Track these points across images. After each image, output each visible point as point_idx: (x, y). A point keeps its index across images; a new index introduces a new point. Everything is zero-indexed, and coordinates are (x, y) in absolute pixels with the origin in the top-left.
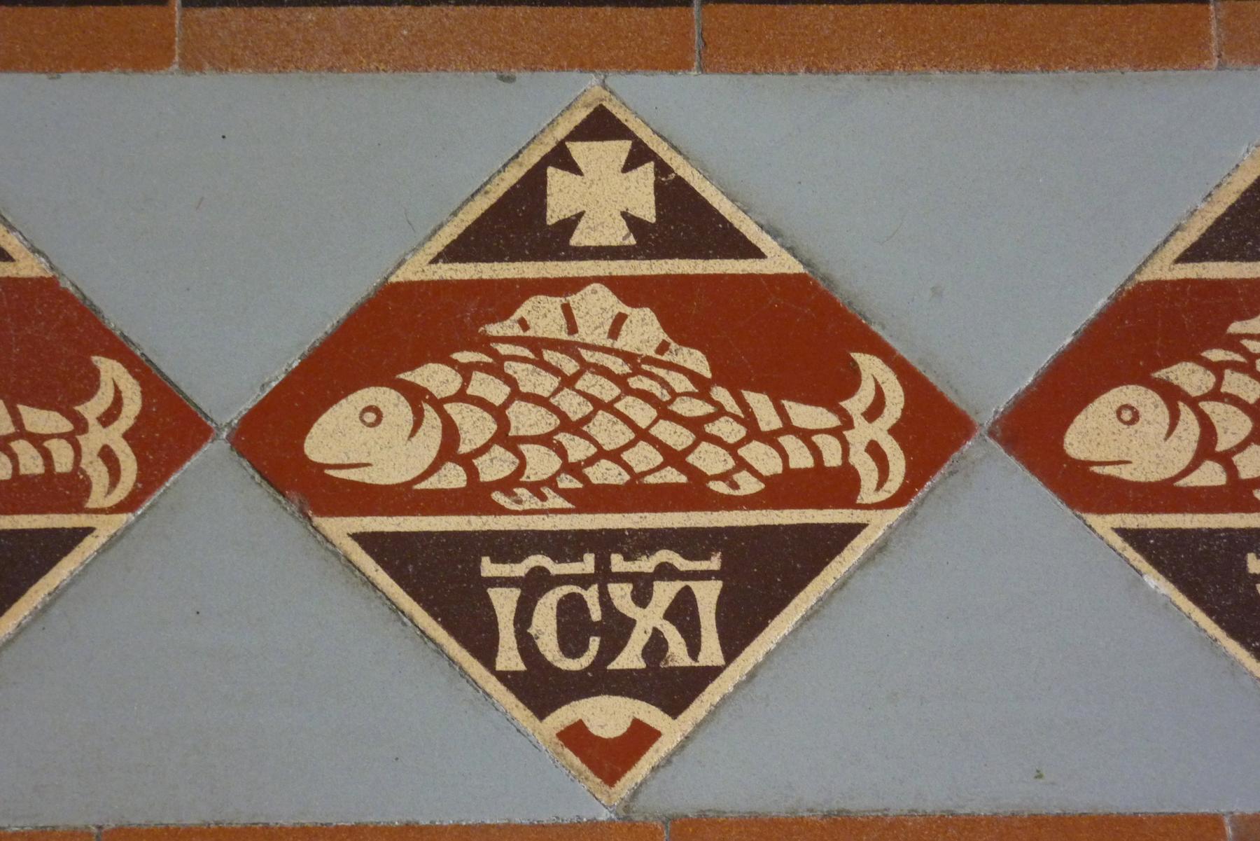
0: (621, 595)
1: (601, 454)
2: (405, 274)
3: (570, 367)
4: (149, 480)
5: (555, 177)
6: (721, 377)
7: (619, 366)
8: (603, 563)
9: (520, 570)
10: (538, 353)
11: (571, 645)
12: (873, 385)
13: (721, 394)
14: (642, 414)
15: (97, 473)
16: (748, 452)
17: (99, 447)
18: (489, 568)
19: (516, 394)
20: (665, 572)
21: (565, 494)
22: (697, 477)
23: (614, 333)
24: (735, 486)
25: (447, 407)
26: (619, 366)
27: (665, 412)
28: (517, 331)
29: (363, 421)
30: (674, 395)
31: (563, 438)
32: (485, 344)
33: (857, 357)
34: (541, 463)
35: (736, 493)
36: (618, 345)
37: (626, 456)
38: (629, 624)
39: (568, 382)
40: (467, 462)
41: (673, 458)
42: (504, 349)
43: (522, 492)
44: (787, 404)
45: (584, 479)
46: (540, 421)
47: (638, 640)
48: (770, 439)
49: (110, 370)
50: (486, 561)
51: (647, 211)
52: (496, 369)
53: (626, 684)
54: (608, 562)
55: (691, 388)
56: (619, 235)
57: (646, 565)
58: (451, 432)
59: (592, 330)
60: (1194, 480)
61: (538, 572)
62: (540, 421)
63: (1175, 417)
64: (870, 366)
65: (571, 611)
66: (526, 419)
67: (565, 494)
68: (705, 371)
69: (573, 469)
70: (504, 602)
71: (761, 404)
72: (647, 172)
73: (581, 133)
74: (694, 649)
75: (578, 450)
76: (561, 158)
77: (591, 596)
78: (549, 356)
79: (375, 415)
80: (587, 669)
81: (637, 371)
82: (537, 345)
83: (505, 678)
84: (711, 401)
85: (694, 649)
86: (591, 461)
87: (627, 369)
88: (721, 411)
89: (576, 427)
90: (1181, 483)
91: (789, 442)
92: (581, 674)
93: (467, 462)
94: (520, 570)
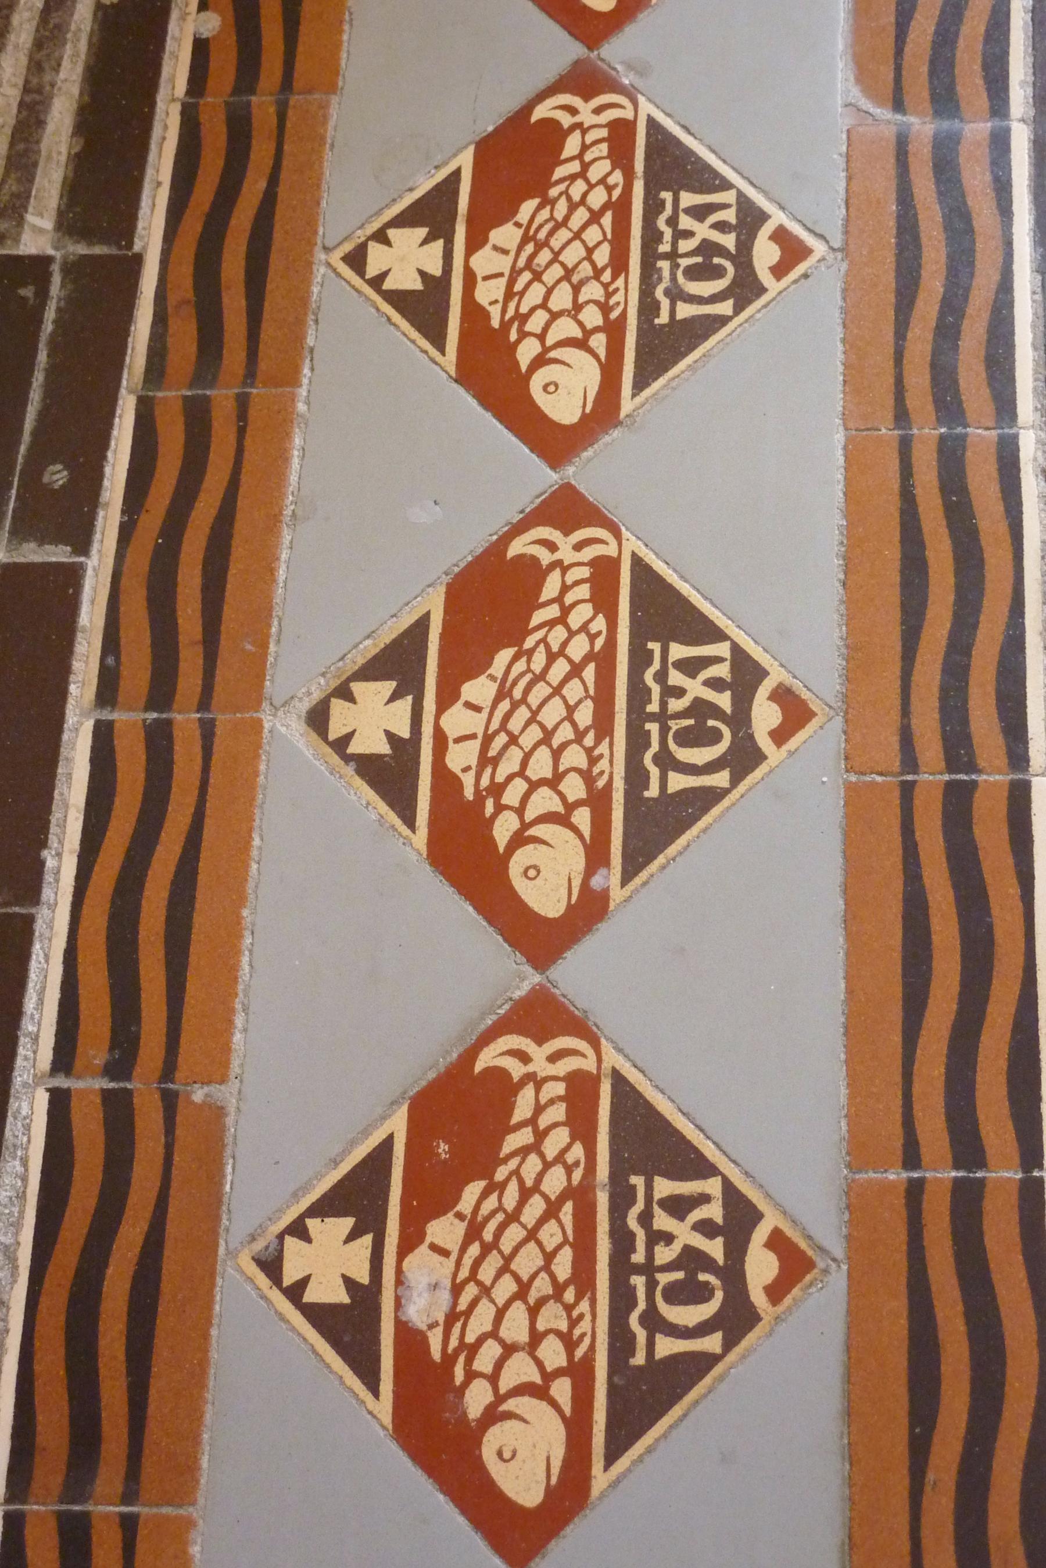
0: (664, 1255)
1: (570, 718)
2: (387, 1419)
3: (502, 739)
4: (615, 87)
5: (310, 1296)
6: (487, 1173)
7: (474, 1250)
8: (638, 1269)
9: (654, 772)
10: (516, 294)
11: (702, 1295)
12: (553, 111)
13: (501, 1173)
14: (514, 1234)
15: (564, 1067)
16: (550, 1153)
17: (573, 552)
18: (653, 791)
19: (494, 1334)
20: (645, 1218)
21: (614, 278)
22: (588, 658)
23: (445, 1253)
24: (577, 1164)
25: (502, 1391)
26: (474, 1250)
27: (542, 677)
28: (439, 1331)
29: (535, 878)
30: (500, 1208)
31: (533, 1297)
32: (449, 1360)
33: (533, 119)
34: (552, 1317)
35: (604, 632)
36: (454, 1248)
37: (572, 703)
38: (687, 1249)
39: (513, 740)
40: (548, 1377)
41: (552, 1211)
42: (454, 1343)
43: (577, 1332)
44: (563, 157)
45: (567, 1283)
46: (518, 1314)
47: (710, 695)
48: (541, 1136)
49: (486, 1059)
50: (647, 794)
51: (388, 687)
52: (473, 1350)
53: (737, 1250)
54: (653, 714)
55: (548, 208)
56: (406, 703)
57: (656, 690)
58: (524, 1389)
59: (476, 723)
60: (586, 830)
61: (643, 1320)
62: (518, 1314)
63: (509, 1415)
64: (517, 547)
65: (676, 1294)
66: (541, 765)
67: (579, 1298)
68: (536, 202)
69: (559, 1290)
70: (666, 1346)
71: (513, 1142)
72: (357, 687)
73: (360, 271)
74: (719, 660)
75: (542, 1286)
76: (341, 745)
77: (664, 1279)
78: (463, 1304)
79: (531, 872)
80: (736, 271)
81: (510, 694)
82: (509, 294)
83: (735, 781)
84: (508, 1179)
85: (719, 660)
86: (574, 724)
87: (507, 701)
88: (516, 1172)
89: (568, 273)
90: (567, 1410)
91: (543, 1122)
92: (734, 735)
93: (548, 1377)
94: (654, 772)
